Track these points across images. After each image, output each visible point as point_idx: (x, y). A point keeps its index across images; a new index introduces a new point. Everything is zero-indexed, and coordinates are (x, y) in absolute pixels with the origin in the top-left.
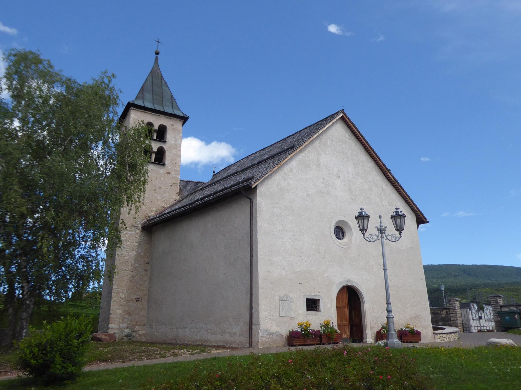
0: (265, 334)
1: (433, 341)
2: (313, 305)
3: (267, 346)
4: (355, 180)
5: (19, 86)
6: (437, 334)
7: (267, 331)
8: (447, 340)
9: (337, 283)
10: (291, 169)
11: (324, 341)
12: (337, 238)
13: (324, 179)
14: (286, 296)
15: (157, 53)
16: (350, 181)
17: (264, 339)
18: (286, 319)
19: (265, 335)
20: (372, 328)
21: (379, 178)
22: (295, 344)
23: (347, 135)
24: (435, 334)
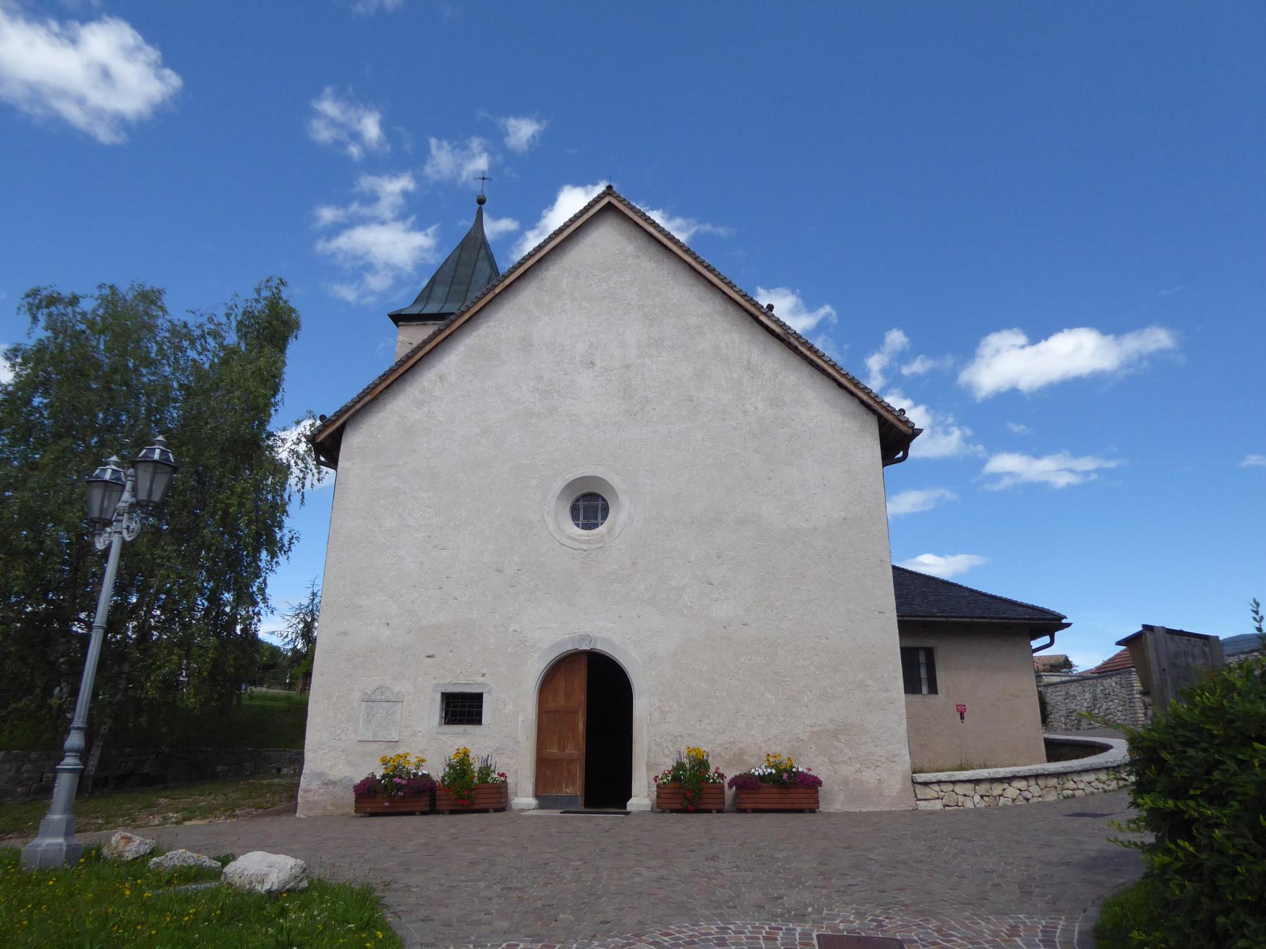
1: (906, 804)
2: (462, 708)
3: (318, 812)
4: (648, 361)
5: (350, 89)
6: (926, 784)
7: (319, 775)
8: (974, 801)
9: (545, 646)
10: (441, 378)
11: (441, 804)
12: (605, 517)
16: (628, 367)
17: (310, 796)
18: (375, 746)
20: (650, 767)
21: (736, 337)
22: (710, 806)
23: (630, 248)
24: (914, 782)
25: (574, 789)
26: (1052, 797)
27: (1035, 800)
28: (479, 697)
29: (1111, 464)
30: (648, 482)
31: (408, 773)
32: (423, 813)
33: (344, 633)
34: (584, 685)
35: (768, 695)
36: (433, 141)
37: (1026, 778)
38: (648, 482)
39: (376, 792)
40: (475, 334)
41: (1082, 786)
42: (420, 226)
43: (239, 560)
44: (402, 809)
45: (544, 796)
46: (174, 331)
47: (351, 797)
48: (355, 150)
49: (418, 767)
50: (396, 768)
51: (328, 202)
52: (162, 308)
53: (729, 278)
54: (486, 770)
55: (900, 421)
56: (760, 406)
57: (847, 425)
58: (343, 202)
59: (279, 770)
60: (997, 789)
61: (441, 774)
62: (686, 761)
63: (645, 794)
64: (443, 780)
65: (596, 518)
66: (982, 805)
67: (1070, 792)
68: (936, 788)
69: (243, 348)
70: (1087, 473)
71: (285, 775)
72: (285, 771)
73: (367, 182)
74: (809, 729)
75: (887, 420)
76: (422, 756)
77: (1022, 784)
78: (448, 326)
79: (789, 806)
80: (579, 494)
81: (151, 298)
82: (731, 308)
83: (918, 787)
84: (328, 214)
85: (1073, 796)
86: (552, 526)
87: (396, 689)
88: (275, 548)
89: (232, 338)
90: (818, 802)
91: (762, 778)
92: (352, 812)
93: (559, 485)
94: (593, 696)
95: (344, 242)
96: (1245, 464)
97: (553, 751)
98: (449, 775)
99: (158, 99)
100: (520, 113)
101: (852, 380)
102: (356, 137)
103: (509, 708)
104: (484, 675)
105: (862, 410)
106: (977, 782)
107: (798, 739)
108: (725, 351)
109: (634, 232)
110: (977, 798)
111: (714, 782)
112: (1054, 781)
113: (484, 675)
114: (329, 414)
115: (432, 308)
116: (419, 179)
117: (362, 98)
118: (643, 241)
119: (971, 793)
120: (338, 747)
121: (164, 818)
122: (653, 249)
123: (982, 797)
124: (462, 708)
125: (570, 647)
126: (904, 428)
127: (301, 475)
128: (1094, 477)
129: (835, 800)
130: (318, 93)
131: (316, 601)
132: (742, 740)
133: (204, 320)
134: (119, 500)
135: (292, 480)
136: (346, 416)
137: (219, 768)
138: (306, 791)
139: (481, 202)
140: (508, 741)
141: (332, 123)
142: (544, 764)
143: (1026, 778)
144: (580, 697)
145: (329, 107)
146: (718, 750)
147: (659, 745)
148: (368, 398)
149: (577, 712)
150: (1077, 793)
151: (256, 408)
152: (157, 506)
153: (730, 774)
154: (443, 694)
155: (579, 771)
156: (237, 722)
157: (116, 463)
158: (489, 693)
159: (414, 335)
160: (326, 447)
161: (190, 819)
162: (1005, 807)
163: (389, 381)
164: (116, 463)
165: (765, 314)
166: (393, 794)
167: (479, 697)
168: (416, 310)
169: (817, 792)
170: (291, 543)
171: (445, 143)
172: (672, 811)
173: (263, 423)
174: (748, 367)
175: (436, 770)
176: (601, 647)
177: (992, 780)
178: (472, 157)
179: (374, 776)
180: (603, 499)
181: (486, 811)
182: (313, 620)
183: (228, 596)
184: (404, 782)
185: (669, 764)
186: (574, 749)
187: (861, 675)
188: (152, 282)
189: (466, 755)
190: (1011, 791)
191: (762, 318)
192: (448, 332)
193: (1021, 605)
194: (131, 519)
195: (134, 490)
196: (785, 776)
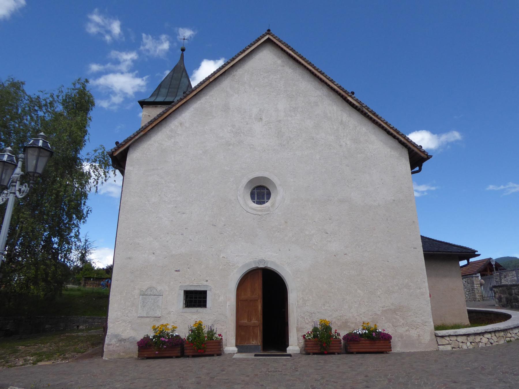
0: (113, 341)
2: (195, 299)
3: (115, 356)
4: (289, 118)
6: (442, 337)
7: (116, 336)
8: (467, 345)
9: (240, 265)
10: (181, 124)
11: (187, 352)
12: (269, 198)
13: (233, 126)
14: (151, 288)
15: (183, 50)
16: (280, 121)
17: (111, 348)
18: (148, 319)
19: (113, 341)
20: (298, 330)
21: (335, 108)
23: (279, 62)
24: (436, 336)
25: (257, 341)
26: (502, 342)
27: (495, 344)
28: (205, 292)
29: (433, 188)
30: (292, 180)
31: (168, 334)
32: (177, 357)
33: (130, 258)
34: (261, 286)
35: (359, 291)
36: (144, 35)
37: (490, 332)
38: (292, 180)
39: (150, 345)
40: (199, 102)
41: (513, 335)
42: (140, 76)
43: (61, 220)
44: (167, 355)
45: (241, 348)
46: (31, 100)
47: (135, 348)
48: (108, 38)
49: (173, 331)
50: (161, 332)
51: (96, 63)
52: (23, 91)
53: (331, 78)
54: (211, 333)
55: (421, 151)
56: (348, 142)
57: (393, 153)
58: (104, 62)
59: (78, 327)
60: (478, 339)
61: (187, 335)
62: (319, 327)
63: (296, 344)
64: (188, 338)
65: (264, 199)
66: (471, 347)
67: (509, 339)
68: (448, 339)
69: (65, 114)
70: (423, 192)
71: (82, 330)
72: (81, 327)
73: (114, 54)
74: (381, 309)
75: (413, 150)
76: (175, 325)
77: (489, 336)
78: (170, 108)
79: (376, 350)
80: (253, 187)
81: (17, 86)
82: (331, 93)
83: (438, 338)
84: (95, 68)
85: (511, 341)
86: (242, 202)
87: (159, 288)
88: (81, 217)
89: (59, 108)
90: (391, 348)
91: (361, 335)
92: (137, 357)
93: (245, 181)
94: (266, 292)
95: (102, 81)
96: (488, 189)
97: (245, 321)
98: (190, 335)
99: (13, 10)
100: (185, 25)
101: (396, 130)
102: (109, 32)
103: (222, 298)
104: (207, 281)
105: (400, 146)
106: (468, 335)
107: (376, 314)
108: (329, 115)
109: (281, 54)
110: (469, 344)
111: (336, 338)
112: (502, 334)
113: (207, 281)
114: (121, 141)
115: (160, 99)
116: (139, 53)
117: (111, 14)
118: (285, 58)
119: (465, 341)
120: (126, 322)
121: (25, 360)
122: (291, 62)
123: (471, 343)
124: (195, 299)
125: (253, 266)
126: (422, 155)
127: (96, 178)
128: (426, 194)
129: (397, 347)
130: (91, 12)
131: (87, 243)
132: (348, 317)
133: (48, 96)
134: (12, 174)
135: (91, 181)
136: (130, 142)
137: (47, 326)
138: (109, 345)
139: (183, 50)
140: (221, 316)
141: (98, 25)
142: (239, 327)
143: (490, 332)
144: (258, 293)
145: (96, 18)
146: (334, 320)
147: (303, 318)
148: (142, 133)
149: (257, 300)
150: (512, 339)
151: (75, 142)
152: (40, 176)
153: (343, 333)
154: (184, 291)
155: (259, 332)
156: (62, 305)
157: (10, 151)
158: (210, 290)
159: (154, 112)
160: (118, 160)
161: (41, 361)
162: (482, 348)
163: (153, 125)
164: (10, 151)
165: (350, 96)
166: (159, 347)
167: (205, 292)
168: (152, 100)
169: (390, 342)
170: (87, 213)
171: (150, 37)
172: (314, 354)
173: (77, 151)
174: (341, 123)
175: (183, 333)
176: (270, 266)
177: (476, 334)
178: (162, 43)
179: (148, 337)
180: (268, 189)
181: (212, 355)
182: (86, 252)
183: (55, 240)
184: (167, 340)
185: (309, 328)
186: (256, 320)
187: (407, 280)
188: (18, 78)
189: (200, 324)
190: (484, 339)
191: (349, 98)
192: (185, 100)
193: (454, 246)
194: (22, 184)
195: (23, 168)
196: (374, 334)
